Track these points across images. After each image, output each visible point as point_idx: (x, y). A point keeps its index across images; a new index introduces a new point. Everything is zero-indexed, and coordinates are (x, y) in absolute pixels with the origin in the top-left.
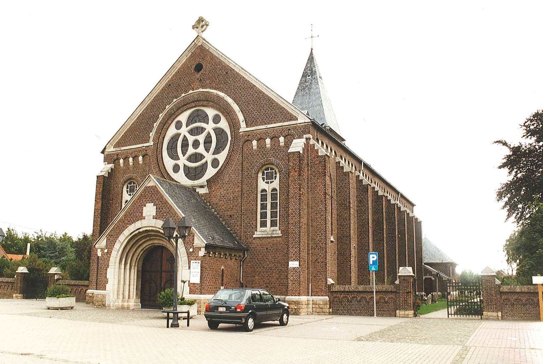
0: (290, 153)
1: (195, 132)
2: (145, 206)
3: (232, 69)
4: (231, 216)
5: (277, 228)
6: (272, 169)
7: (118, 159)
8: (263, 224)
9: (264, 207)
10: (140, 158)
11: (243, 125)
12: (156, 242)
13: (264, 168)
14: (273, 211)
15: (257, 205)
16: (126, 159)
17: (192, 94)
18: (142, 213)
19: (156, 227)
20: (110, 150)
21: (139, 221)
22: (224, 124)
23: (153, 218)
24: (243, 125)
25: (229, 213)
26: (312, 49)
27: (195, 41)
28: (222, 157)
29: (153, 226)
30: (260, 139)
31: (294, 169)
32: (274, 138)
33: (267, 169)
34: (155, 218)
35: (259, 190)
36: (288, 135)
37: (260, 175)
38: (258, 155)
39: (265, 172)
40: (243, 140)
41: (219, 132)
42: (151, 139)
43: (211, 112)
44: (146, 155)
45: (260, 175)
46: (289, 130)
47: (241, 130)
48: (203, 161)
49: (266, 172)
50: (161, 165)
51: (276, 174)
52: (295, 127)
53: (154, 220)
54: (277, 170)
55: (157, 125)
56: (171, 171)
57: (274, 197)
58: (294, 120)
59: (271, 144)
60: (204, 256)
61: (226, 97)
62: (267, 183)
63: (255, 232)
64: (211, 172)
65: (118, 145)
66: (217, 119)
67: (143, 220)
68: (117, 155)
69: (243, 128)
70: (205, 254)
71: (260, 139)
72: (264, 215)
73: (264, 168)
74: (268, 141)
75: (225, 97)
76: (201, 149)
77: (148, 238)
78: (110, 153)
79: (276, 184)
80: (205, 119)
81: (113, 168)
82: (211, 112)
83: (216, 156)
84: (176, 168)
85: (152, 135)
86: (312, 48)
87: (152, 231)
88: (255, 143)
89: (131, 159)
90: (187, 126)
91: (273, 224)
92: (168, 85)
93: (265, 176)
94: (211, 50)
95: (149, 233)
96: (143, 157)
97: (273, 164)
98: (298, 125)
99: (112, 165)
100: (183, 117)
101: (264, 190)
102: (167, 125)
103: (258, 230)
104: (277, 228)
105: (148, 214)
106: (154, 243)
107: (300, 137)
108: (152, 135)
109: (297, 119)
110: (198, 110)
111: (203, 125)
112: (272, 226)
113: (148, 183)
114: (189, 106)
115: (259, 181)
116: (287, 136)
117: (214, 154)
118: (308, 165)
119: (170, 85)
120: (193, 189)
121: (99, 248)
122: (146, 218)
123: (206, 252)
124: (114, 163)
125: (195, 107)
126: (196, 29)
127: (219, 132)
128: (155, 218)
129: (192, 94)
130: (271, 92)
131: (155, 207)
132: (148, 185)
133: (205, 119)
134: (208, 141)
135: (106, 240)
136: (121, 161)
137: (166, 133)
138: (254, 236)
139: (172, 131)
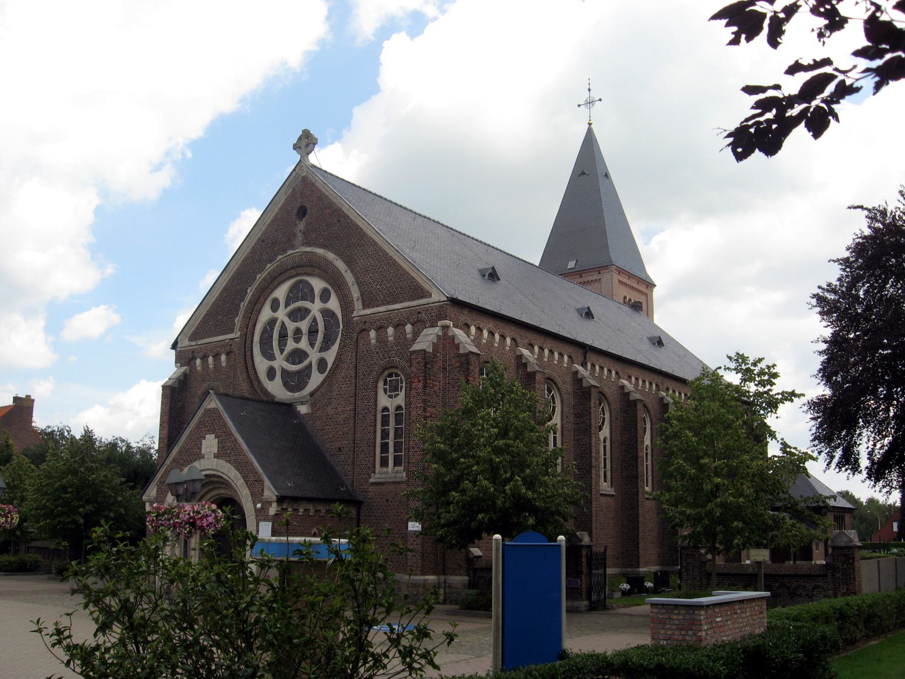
0: (414, 352)
1: (298, 315)
2: (204, 438)
3: (346, 214)
4: (340, 449)
5: (402, 468)
6: (397, 375)
7: (194, 358)
8: (384, 462)
9: (385, 435)
10: (223, 358)
11: (358, 305)
12: (222, 491)
13: (386, 373)
14: (397, 442)
15: (375, 432)
16: (204, 358)
17: (292, 255)
18: (200, 448)
19: (218, 471)
20: (183, 345)
21: (197, 461)
22: (334, 304)
23: (214, 457)
24: (358, 305)
25: (338, 445)
26: (590, 124)
27: (297, 170)
28: (331, 356)
29: (214, 468)
30: (381, 329)
31: (418, 377)
32: (399, 326)
33: (390, 375)
34: (217, 456)
35: (380, 408)
36: (418, 321)
37: (381, 384)
38: (377, 353)
39: (388, 379)
40: (357, 329)
41: (328, 314)
42: (237, 327)
43: (318, 284)
44: (231, 352)
45: (381, 384)
46: (419, 313)
47: (355, 314)
48: (306, 363)
49: (390, 380)
50: (250, 368)
51: (402, 383)
52: (427, 309)
53: (215, 459)
54: (403, 378)
55: (246, 305)
56: (263, 376)
57: (398, 419)
58: (426, 297)
59: (395, 336)
60: (276, 515)
61: (336, 260)
62: (390, 397)
63: (373, 474)
64: (316, 379)
65: (194, 336)
66: (325, 296)
67: (202, 460)
68: (193, 352)
69: (359, 311)
70: (278, 512)
71: (381, 329)
72: (385, 448)
73: (386, 373)
74: (390, 330)
75: (334, 261)
76: (304, 344)
77: (211, 487)
78: (184, 349)
79: (400, 400)
80: (309, 295)
81: (188, 372)
82: (318, 284)
83: (323, 354)
84: (271, 373)
85: (238, 320)
86: (591, 122)
87: (214, 476)
88: (373, 334)
89: (211, 359)
90: (286, 307)
91: (397, 462)
92: (261, 241)
93: (387, 387)
94: (317, 184)
95: (212, 479)
96: (227, 354)
97: (397, 368)
98: (430, 305)
99: (185, 368)
100: (281, 292)
101: (385, 409)
102: (258, 305)
103: (377, 471)
104: (402, 468)
105: (208, 450)
106: (220, 494)
107: (433, 325)
108: (238, 320)
109: (430, 296)
110: (300, 281)
111: (307, 304)
112: (395, 465)
113: (209, 403)
114: (287, 274)
115: (378, 395)
116: (416, 322)
117: (322, 352)
118: (445, 369)
119: (263, 241)
120: (289, 407)
121: (147, 501)
122: (206, 457)
123: (280, 509)
124: (188, 365)
125: (297, 275)
126: (298, 149)
127: (328, 314)
128: (217, 456)
129: (292, 255)
130: (396, 252)
131: (217, 440)
132: (209, 407)
133: (309, 295)
134: (313, 332)
135: (156, 489)
136: (198, 362)
137: (257, 318)
138: (371, 480)
139: (266, 314)
